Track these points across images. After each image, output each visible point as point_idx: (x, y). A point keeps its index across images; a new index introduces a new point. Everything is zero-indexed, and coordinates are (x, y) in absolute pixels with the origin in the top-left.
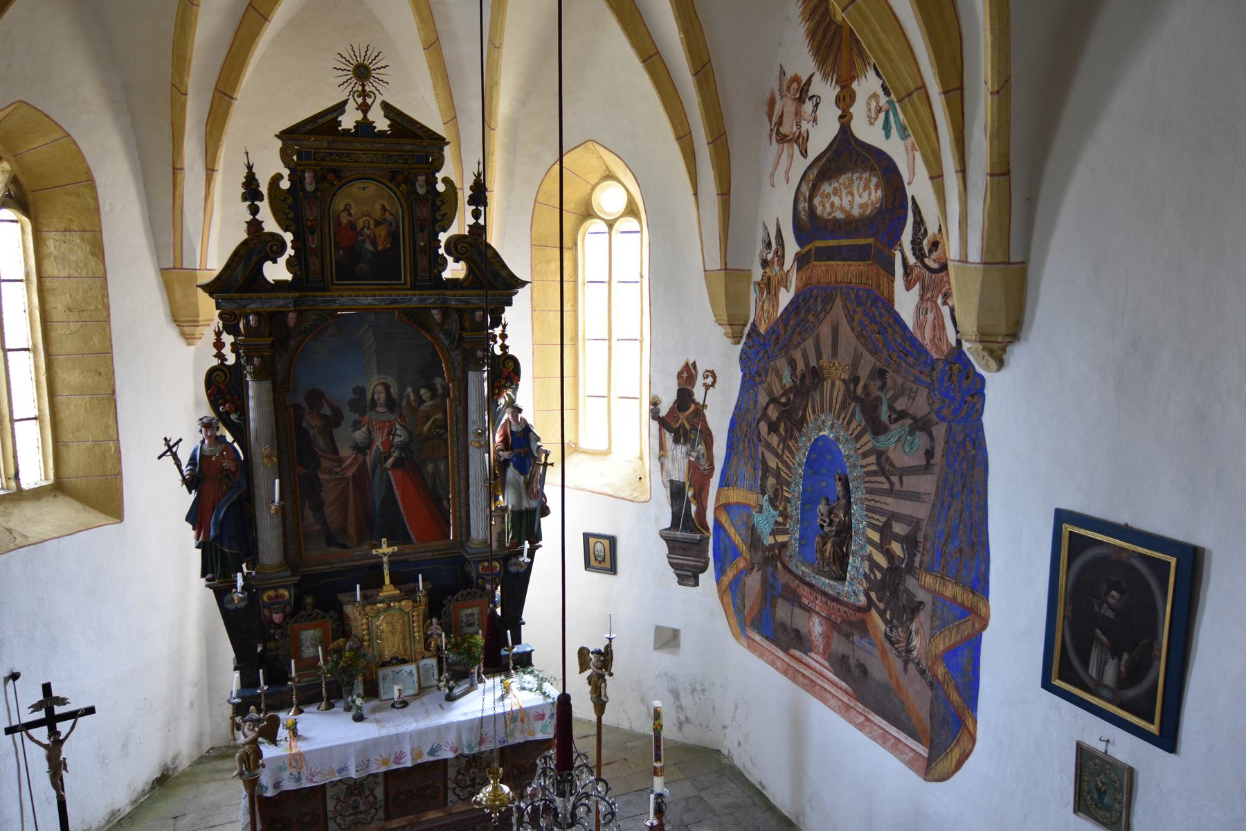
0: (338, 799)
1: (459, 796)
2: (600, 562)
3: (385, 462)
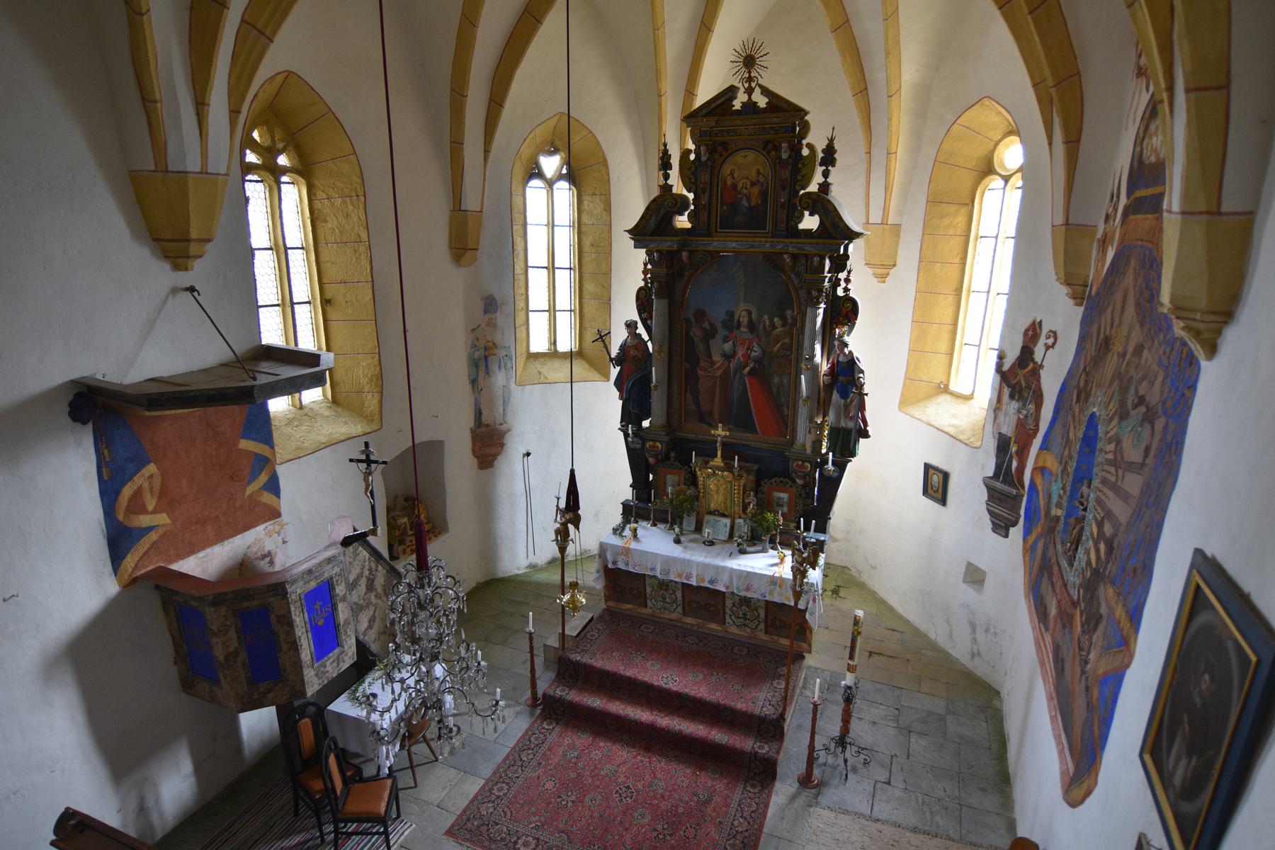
0: (653, 587)
1: (734, 622)
2: (935, 492)
3: (743, 370)
